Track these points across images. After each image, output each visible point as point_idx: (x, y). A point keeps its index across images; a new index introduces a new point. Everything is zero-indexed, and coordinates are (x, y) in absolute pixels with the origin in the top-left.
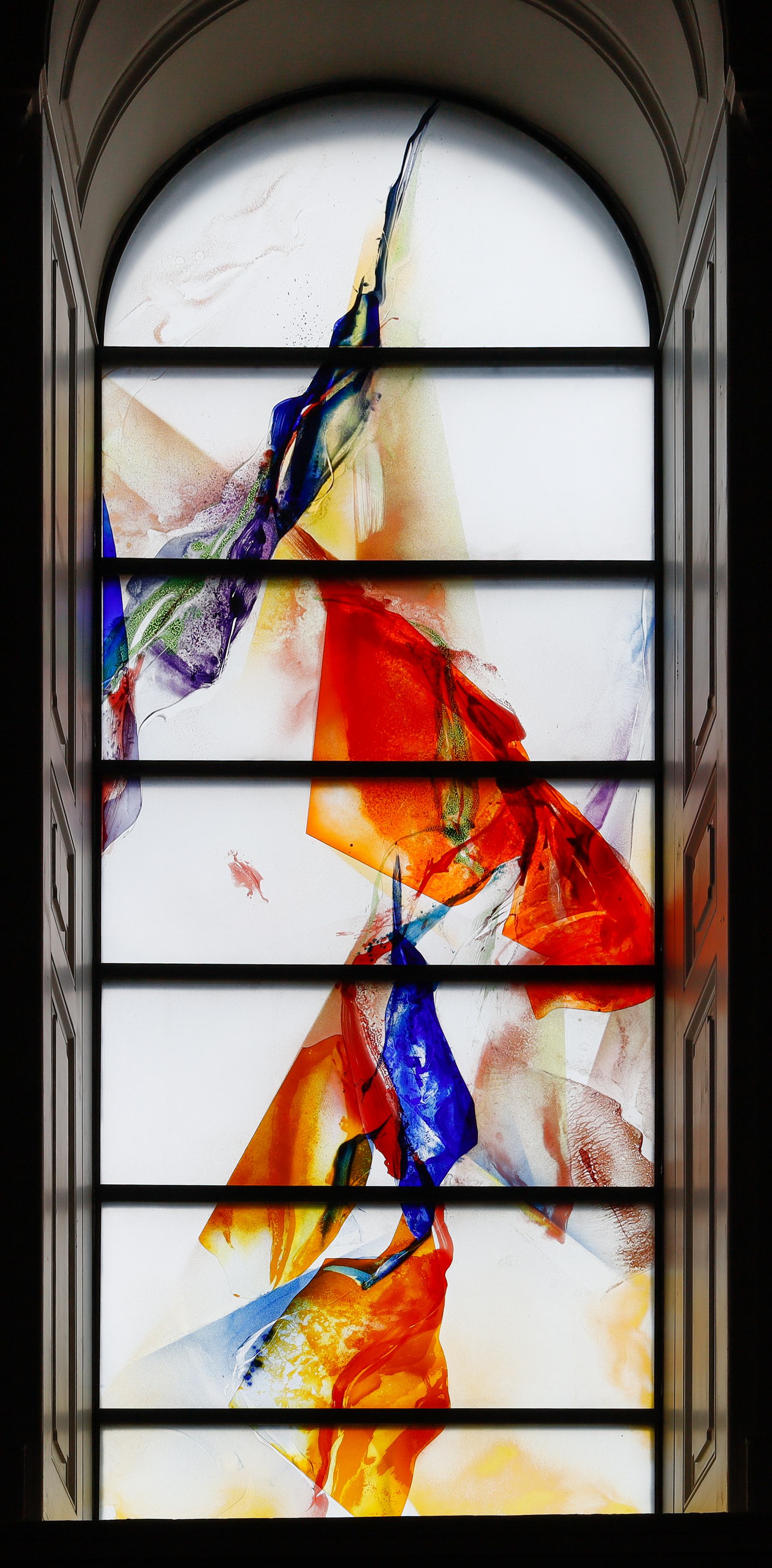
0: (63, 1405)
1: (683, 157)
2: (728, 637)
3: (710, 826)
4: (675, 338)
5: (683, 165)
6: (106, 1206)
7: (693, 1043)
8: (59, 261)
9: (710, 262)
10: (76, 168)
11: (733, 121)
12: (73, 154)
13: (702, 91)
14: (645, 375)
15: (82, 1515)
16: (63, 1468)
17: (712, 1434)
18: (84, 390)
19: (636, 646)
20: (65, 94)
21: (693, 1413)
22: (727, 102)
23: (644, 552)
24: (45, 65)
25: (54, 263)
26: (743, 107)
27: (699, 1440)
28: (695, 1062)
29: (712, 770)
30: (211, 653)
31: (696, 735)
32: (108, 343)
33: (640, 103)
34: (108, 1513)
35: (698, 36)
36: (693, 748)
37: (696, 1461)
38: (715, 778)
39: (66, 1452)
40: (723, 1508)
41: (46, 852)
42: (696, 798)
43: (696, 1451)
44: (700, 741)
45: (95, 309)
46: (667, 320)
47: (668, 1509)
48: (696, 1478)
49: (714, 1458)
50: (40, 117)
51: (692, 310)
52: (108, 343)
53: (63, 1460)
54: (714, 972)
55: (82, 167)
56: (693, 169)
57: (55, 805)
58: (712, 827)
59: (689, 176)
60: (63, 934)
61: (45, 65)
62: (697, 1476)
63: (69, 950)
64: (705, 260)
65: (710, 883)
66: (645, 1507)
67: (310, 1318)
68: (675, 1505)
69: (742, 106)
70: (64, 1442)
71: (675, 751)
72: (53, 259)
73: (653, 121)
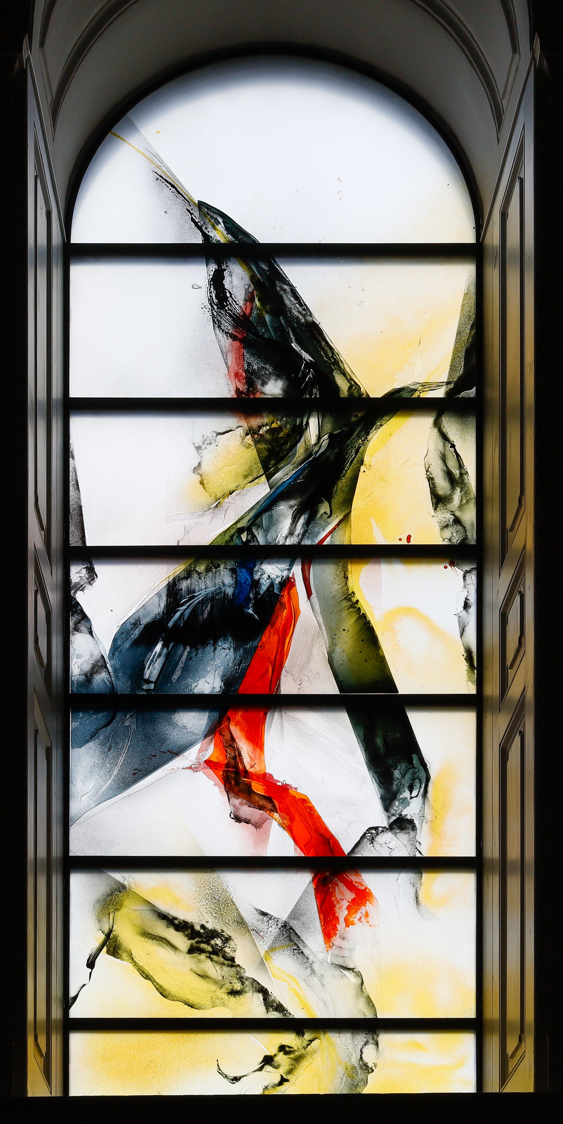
0: (42, 852)
2: (535, 757)
3: (520, 592)
4: (493, 237)
6: (73, 873)
7: (507, 750)
8: (39, 176)
9: (520, 177)
10: (50, 98)
11: (539, 73)
12: (48, 90)
13: (515, 48)
15: (56, 1092)
16: (41, 1061)
17: (522, 640)
20: (42, 44)
21: (507, 1022)
23: (470, 1013)
24: (27, 35)
25: (36, 177)
27: (511, 1045)
28: (509, 764)
29: (521, 551)
30: (149, 164)
32: (73, 241)
34: (76, 1090)
37: (509, 531)
39: (44, 1050)
43: (510, 1051)
45: (64, 200)
46: (486, 225)
48: (510, 1070)
50: (25, 72)
51: (507, 213)
52: (73, 241)
54: (523, 556)
55: (54, 99)
56: (509, 105)
58: (522, 593)
60: (43, 533)
61: (27, 35)
62: (511, 1067)
63: (47, 544)
64: (516, 176)
65: (520, 1032)
66: (469, 1087)
68: (493, 1086)
71: (492, 851)
72: (35, 174)
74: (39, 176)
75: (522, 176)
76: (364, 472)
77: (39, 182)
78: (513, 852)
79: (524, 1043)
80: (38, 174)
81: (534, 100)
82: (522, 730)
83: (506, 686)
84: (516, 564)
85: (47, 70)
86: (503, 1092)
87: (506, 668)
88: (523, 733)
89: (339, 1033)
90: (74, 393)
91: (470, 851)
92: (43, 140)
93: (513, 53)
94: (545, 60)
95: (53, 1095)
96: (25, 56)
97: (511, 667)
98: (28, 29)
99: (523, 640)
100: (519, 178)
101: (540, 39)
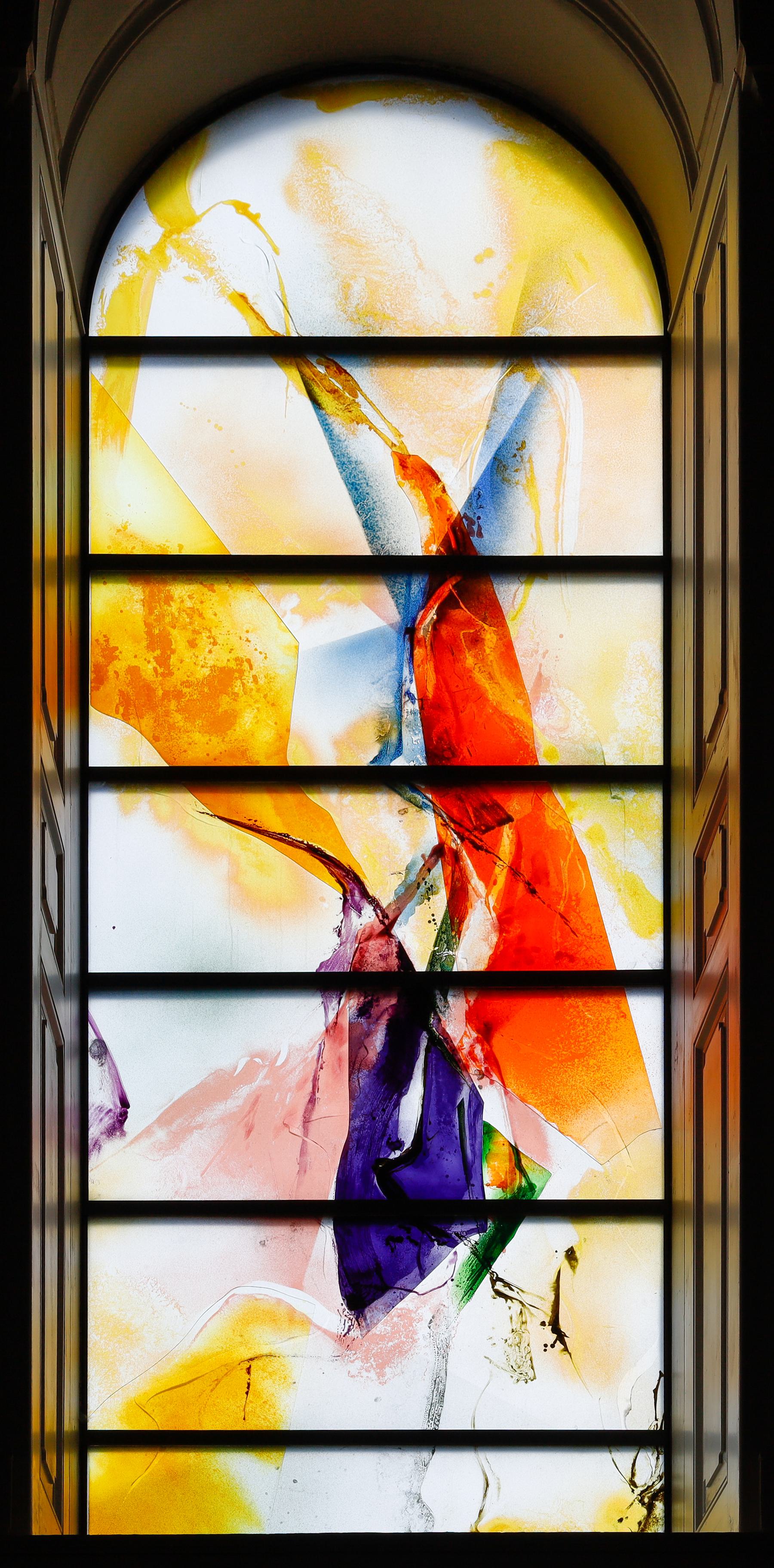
1: (696, 144)
3: (722, 827)
4: (685, 329)
5: (697, 152)
6: (97, 581)
7: (704, 1052)
8: (47, 242)
11: (745, 98)
13: (717, 75)
14: (653, 364)
15: (69, 1529)
16: (50, 1487)
18: (71, 375)
19: (484, 110)
22: (738, 78)
24: (32, 45)
25: (43, 244)
26: (755, 82)
27: (710, 1465)
31: (707, 926)
33: (657, 92)
34: (94, 1529)
35: (716, 26)
36: (703, 746)
37: (708, 936)
38: (726, 777)
39: (54, 1475)
40: (736, 1529)
41: (35, 1030)
42: (705, 802)
43: (707, 1476)
44: (711, 933)
47: (677, 1529)
49: (725, 1483)
53: (50, 1480)
54: (725, 187)
56: (706, 159)
57: (45, 1002)
58: (725, 828)
59: (702, 163)
60: (52, 936)
61: (32, 45)
64: (716, 243)
67: (234, 662)
68: (685, 1524)
69: (754, 83)
70: (52, 1460)
73: (666, 104)
74: (47, 242)
75: (723, 241)
76: (512, 1377)
77: (46, 251)
78: (712, 1193)
79: (726, 1464)
80: (45, 240)
81: (741, 1014)
82: (724, 1021)
83: (704, 959)
84: (717, 787)
85: (60, 136)
86: (700, 1532)
87: (703, 1485)
88: (724, 1025)
89: (475, 1450)
90: (95, 966)
91: (655, 549)
92: (53, 201)
93: (714, 81)
94: (754, 79)
95: (66, 1533)
96: (28, 73)
97: (710, 739)
98: (29, 35)
99: (725, 695)
100: (719, 244)
101: (746, 50)
